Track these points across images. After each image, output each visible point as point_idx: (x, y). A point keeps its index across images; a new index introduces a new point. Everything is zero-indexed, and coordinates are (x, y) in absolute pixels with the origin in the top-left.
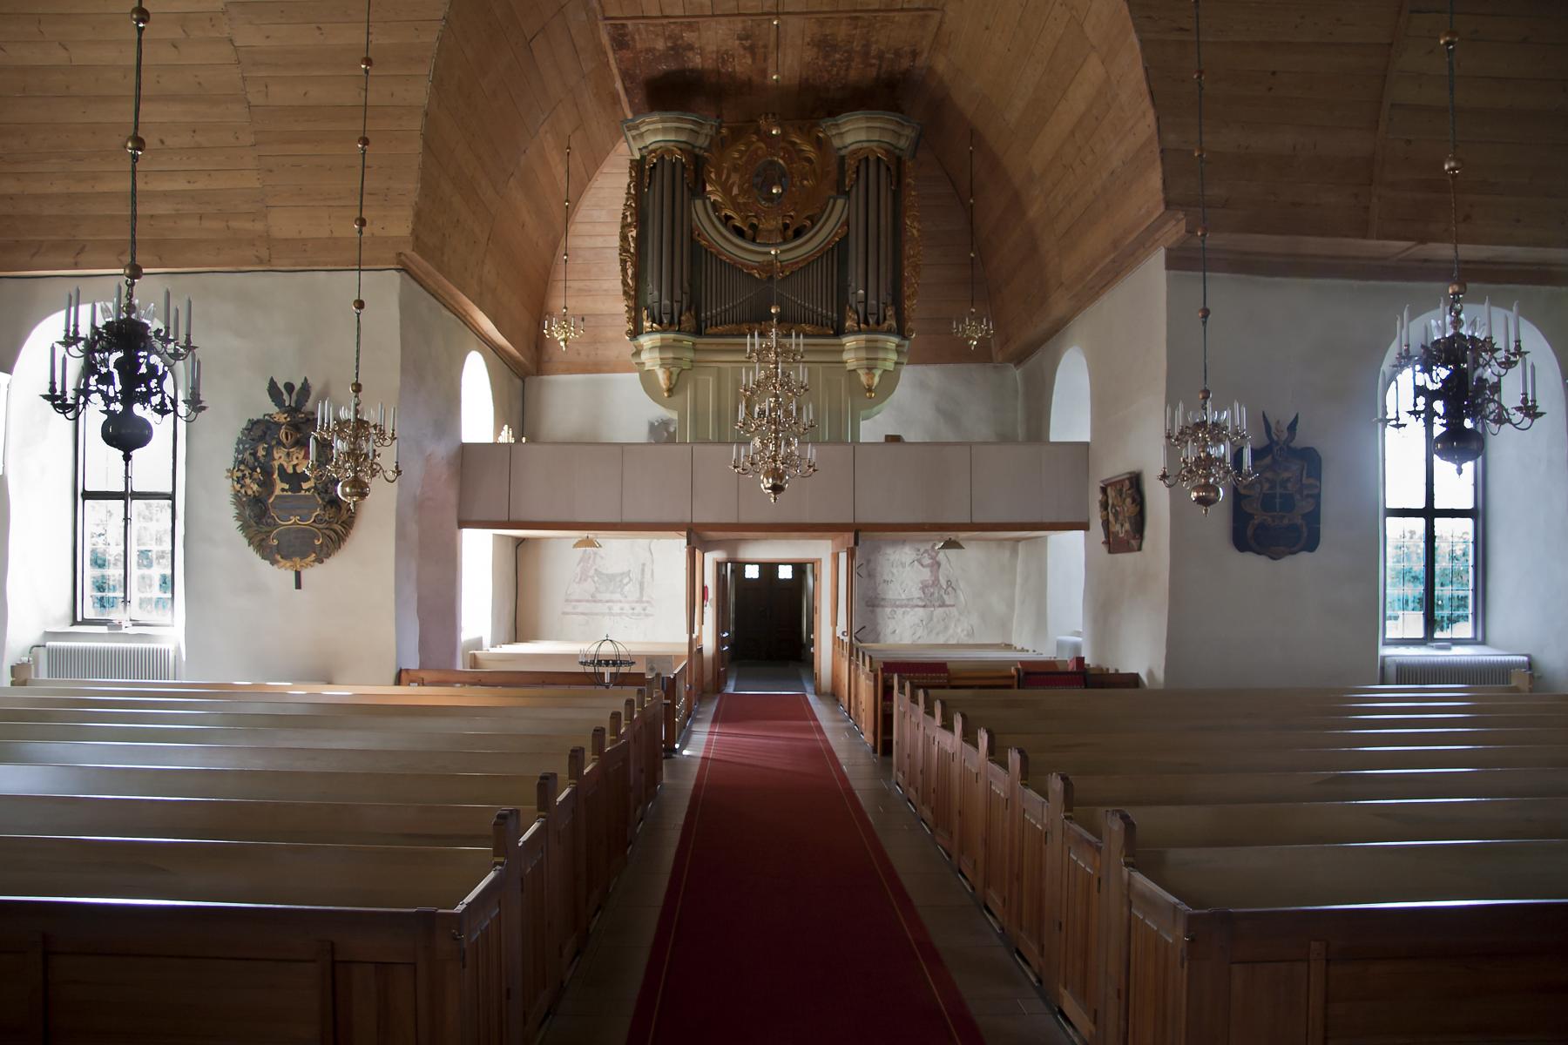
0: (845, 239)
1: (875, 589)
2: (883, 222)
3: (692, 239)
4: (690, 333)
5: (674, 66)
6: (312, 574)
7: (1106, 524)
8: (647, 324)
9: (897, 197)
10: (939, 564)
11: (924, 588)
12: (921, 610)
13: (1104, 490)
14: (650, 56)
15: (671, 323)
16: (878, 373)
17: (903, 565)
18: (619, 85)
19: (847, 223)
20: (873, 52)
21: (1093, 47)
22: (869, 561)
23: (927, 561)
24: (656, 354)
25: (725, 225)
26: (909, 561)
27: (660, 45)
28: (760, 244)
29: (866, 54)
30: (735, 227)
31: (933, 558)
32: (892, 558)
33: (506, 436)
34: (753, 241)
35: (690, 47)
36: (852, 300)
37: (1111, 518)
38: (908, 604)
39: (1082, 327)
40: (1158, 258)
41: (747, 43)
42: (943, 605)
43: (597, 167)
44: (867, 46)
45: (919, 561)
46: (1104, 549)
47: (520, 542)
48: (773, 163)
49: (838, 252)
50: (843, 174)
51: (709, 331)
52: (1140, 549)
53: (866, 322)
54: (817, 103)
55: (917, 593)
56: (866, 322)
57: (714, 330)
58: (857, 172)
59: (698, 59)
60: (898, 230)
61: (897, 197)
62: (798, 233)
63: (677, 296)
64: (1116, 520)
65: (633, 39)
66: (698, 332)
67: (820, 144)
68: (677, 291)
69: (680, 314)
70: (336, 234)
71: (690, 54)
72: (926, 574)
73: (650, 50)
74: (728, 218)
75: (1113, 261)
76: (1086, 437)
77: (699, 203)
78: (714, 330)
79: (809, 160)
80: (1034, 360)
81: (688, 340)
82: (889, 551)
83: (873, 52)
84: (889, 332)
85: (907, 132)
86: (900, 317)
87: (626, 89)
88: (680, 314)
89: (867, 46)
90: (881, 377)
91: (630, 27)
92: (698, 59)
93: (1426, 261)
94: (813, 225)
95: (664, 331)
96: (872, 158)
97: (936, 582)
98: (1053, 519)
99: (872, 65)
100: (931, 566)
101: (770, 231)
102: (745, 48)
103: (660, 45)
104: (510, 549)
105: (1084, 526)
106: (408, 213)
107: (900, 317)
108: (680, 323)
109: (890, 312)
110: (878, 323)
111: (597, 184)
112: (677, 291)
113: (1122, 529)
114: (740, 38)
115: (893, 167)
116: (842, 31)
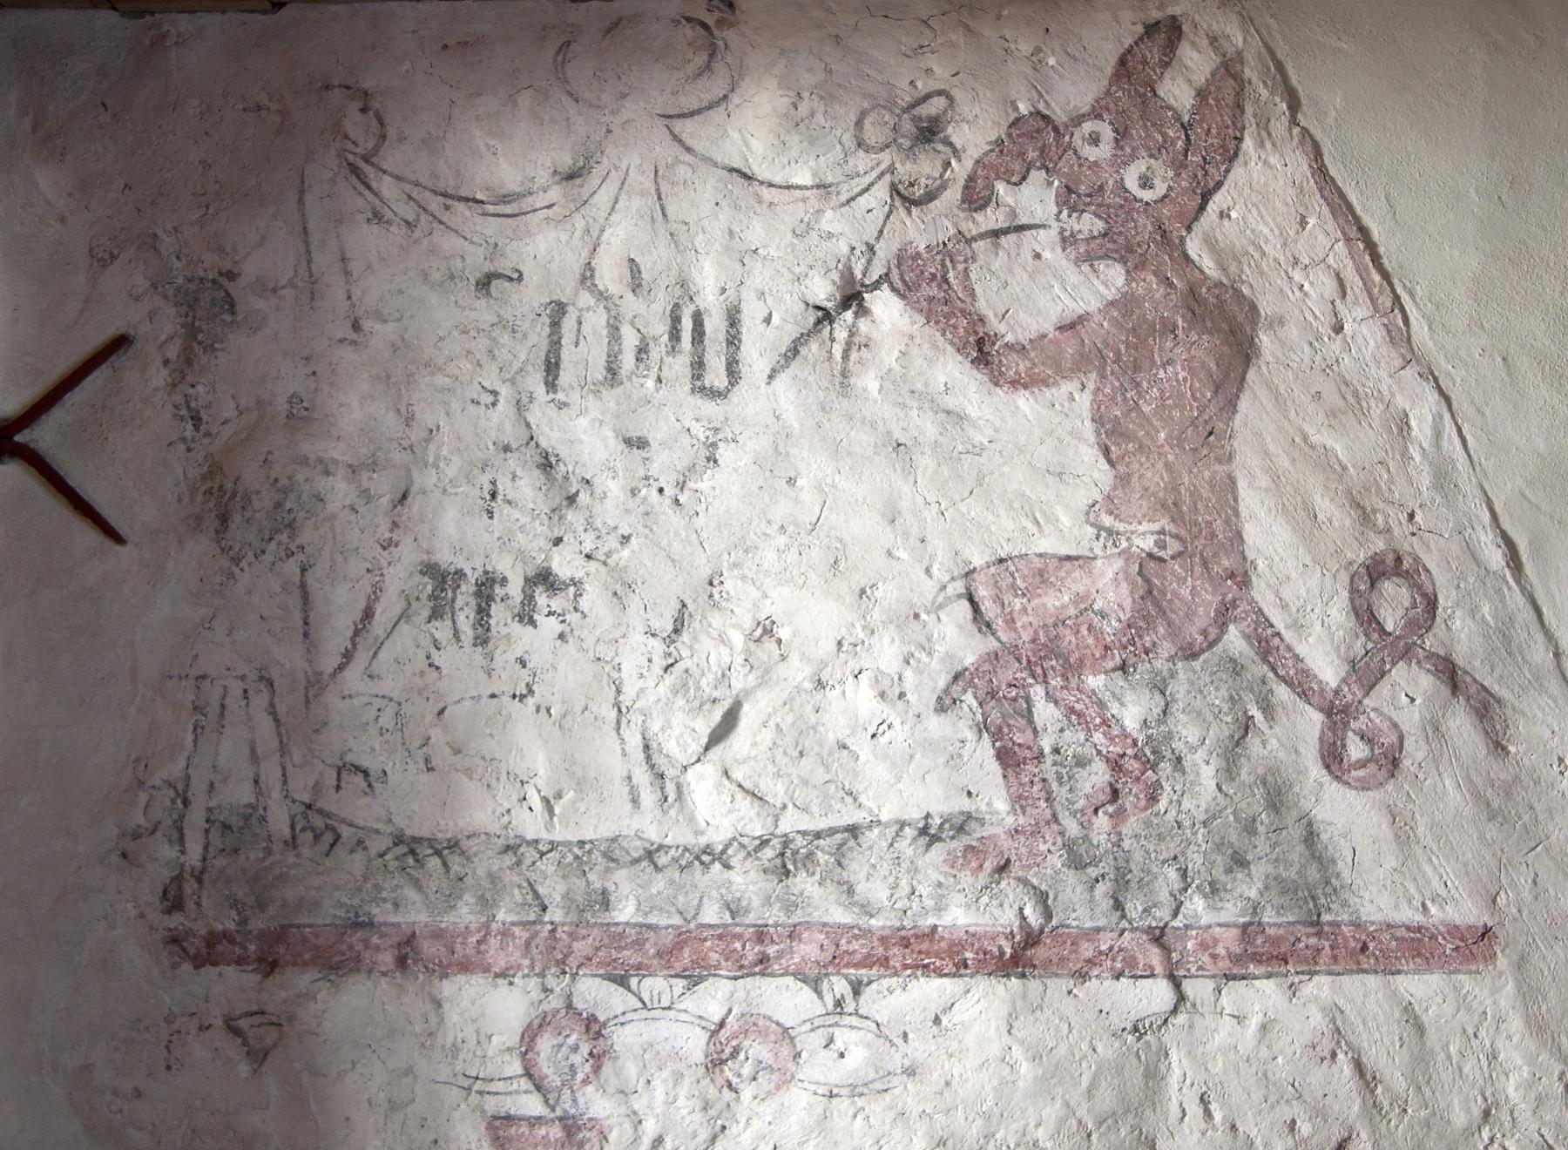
1: (298, 704)
6: (1266, 307)
10: (1227, 327)
11: (1013, 674)
12: (981, 1005)
17: (703, 346)
22: (210, 305)
23: (1046, 282)
26: (781, 291)
31: (1131, 238)
32: (545, 250)
38: (796, 926)
42: (1306, 934)
45: (935, 287)
55: (912, 766)
72: (1038, 479)
82: (513, 155)
93: (1357, 614)
97: (1191, 586)
100: (1105, 357)
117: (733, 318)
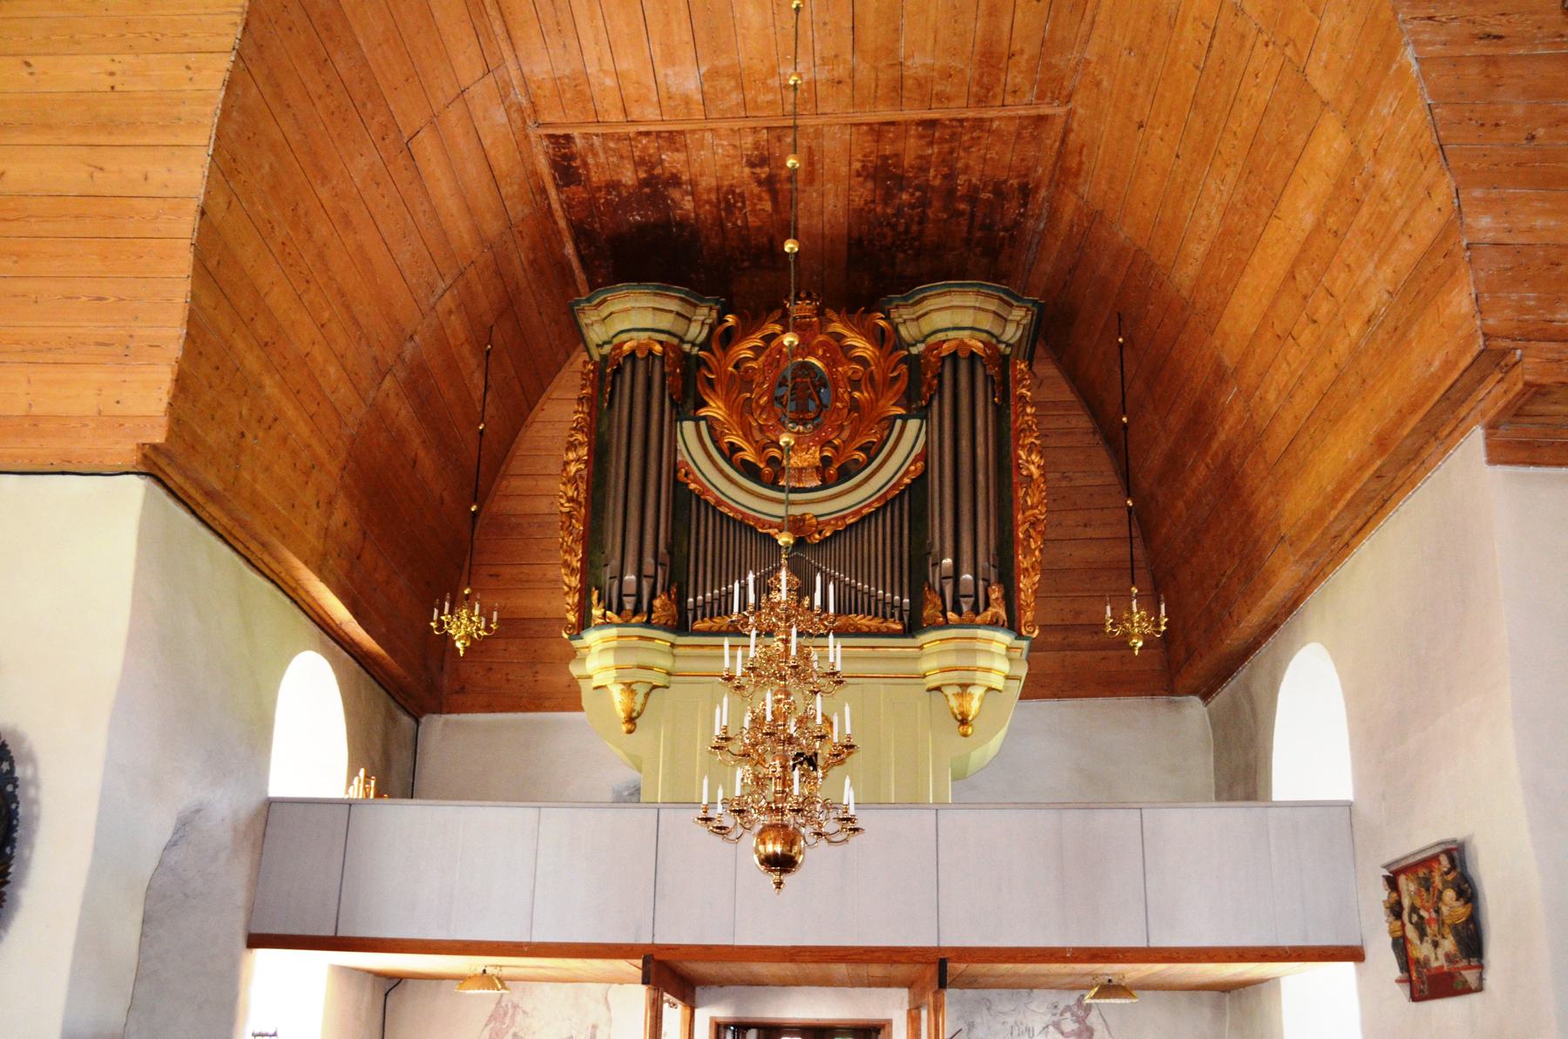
0: (921, 480)
2: (980, 451)
3: (676, 481)
4: (665, 628)
5: (652, 215)
7: (1400, 945)
8: (597, 612)
9: (1001, 414)
10: (1090, 1031)
13: (1392, 882)
14: (613, 197)
15: (637, 611)
16: (977, 692)
18: (569, 249)
19: (924, 456)
20: (961, 191)
21: (1325, 104)
24: (609, 660)
25: (729, 461)
27: (628, 176)
28: (782, 489)
29: (951, 192)
30: (745, 462)
31: (1081, 1021)
33: (356, 792)
34: (774, 485)
35: (675, 181)
36: (934, 577)
37: (1411, 933)
39: (1320, 609)
40: (1475, 440)
41: (763, 172)
43: (543, 389)
44: (950, 177)
45: (1057, 1025)
46: (1402, 993)
47: (392, 983)
48: (806, 366)
49: (911, 499)
50: (921, 381)
51: (699, 625)
52: (1480, 989)
53: (957, 608)
54: (877, 264)
56: (957, 608)
57: (707, 624)
58: (940, 376)
59: (688, 203)
60: (1004, 466)
61: (1001, 414)
62: (845, 474)
63: (649, 568)
64: (1422, 934)
65: (585, 164)
66: (680, 625)
67: (879, 338)
68: (649, 560)
69: (653, 596)
70: (35, 411)
71: (676, 194)
73: (613, 186)
74: (734, 448)
75: (1378, 476)
76: (1345, 793)
77: (688, 426)
78: (707, 624)
79: (862, 361)
80: (1242, 673)
81: (663, 638)
83: (961, 191)
84: (994, 624)
85: (1018, 314)
86: (1010, 599)
87: (581, 258)
88: (653, 596)
89: (950, 177)
90: (982, 700)
91: (579, 143)
92: (688, 203)
94: (870, 460)
95: (626, 624)
96: (963, 354)
98: (1298, 942)
99: (962, 213)
101: (800, 470)
102: (760, 182)
103: (628, 176)
104: (368, 996)
105: (1354, 954)
106: (163, 377)
107: (1010, 599)
108: (651, 610)
109: (995, 594)
110: (975, 610)
111: (541, 416)
112: (649, 560)
113: (1437, 953)
114: (752, 165)
115: (995, 366)
116: (911, 149)
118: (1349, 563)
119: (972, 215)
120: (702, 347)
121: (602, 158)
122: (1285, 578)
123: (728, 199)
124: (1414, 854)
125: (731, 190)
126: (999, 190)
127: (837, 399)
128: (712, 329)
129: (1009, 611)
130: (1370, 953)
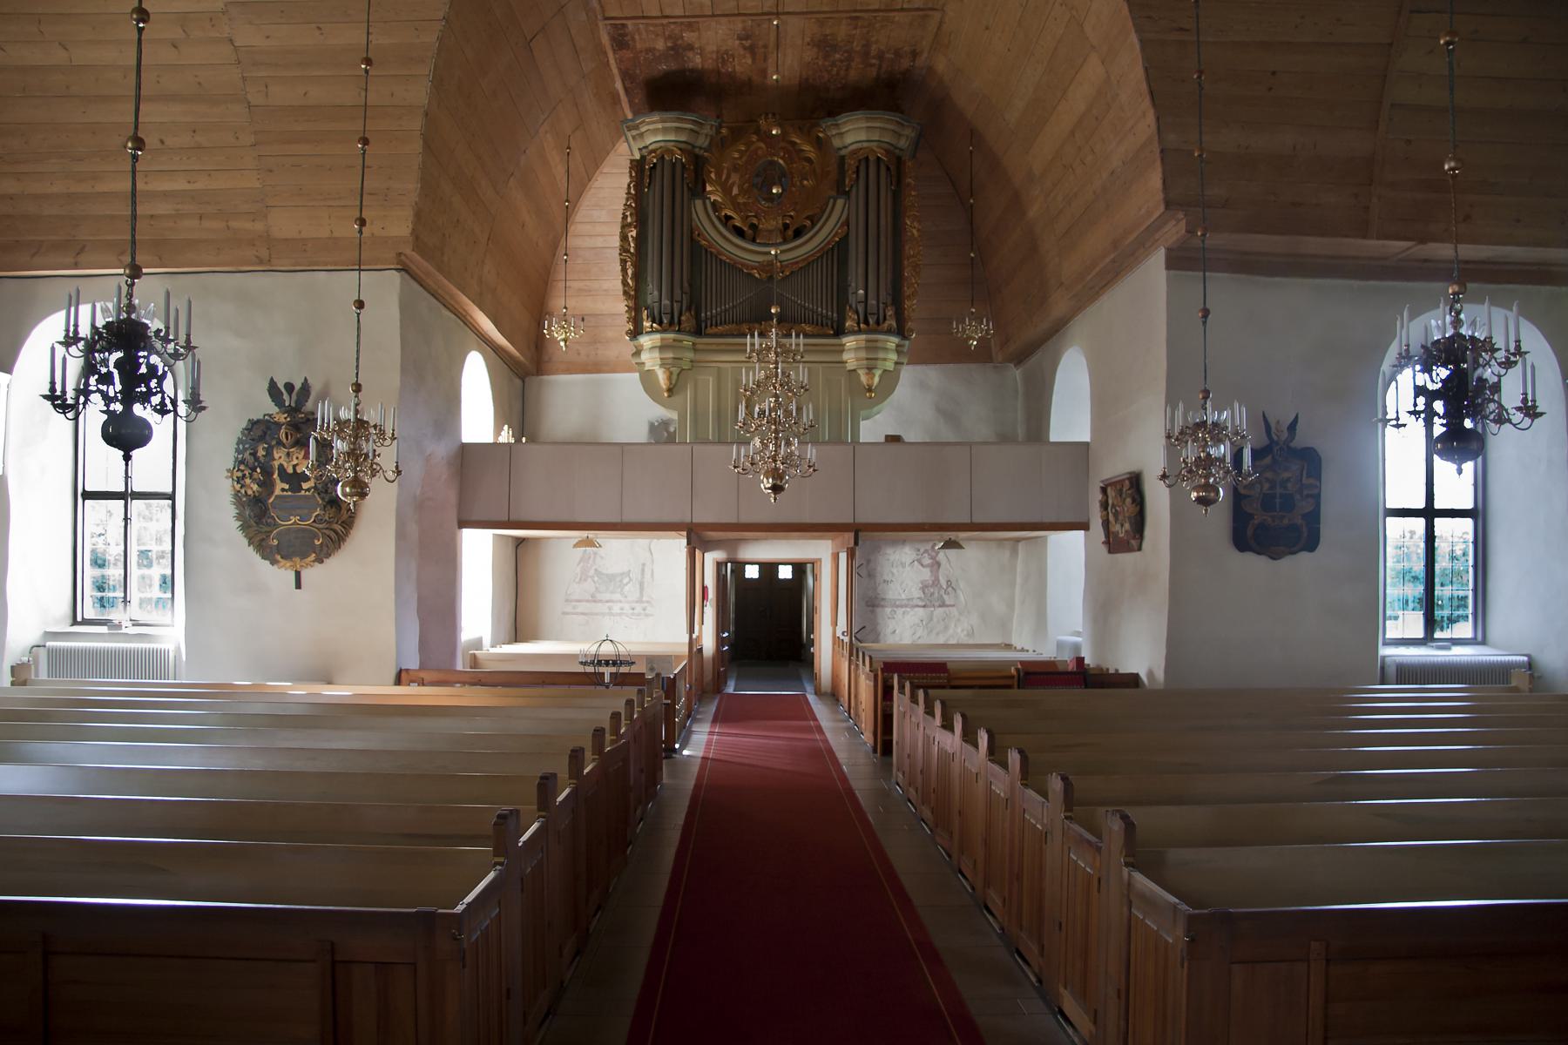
0: (845, 239)
1: (875, 589)
2: (883, 222)
3: (692, 239)
4: (690, 333)
5: (674, 66)
6: (311, 574)
7: (1106, 524)
8: (647, 324)
9: (897, 197)
10: (939, 564)
11: (924, 588)
12: (921, 610)
13: (1104, 490)
14: (650, 56)
15: (671, 323)
16: (878, 373)
17: (903, 565)
18: (619, 85)
19: (847, 223)
21: (1093, 47)
22: (869, 561)
23: (927, 561)
24: (656, 354)
25: (725, 225)
26: (909, 561)
27: (660, 45)
28: (760, 244)
29: (866, 54)
30: (735, 227)
31: (933, 558)
32: (892, 558)
33: (506, 436)
34: (753, 241)
35: (690, 47)
36: (852, 300)
37: (1111, 518)
38: (908, 604)
39: (1081, 327)
40: (1158, 258)
41: (747, 43)
42: (943, 605)
43: (597, 167)
44: (867, 46)
45: (919, 561)
46: (1104, 549)
47: (520, 542)
48: (772, 163)
49: (838, 252)
50: (843, 174)
51: (709, 331)
52: (1140, 549)
53: (866, 322)
54: (817, 103)
55: (917, 593)
56: (866, 322)
58: (857, 172)
59: (698, 59)
60: (898, 230)
61: (897, 197)
62: (798, 233)
63: (677, 296)
64: (1116, 520)
65: (633, 39)
66: (698, 332)
67: (820, 144)
68: (677, 292)
69: (680, 314)
70: (336, 234)
71: (690, 54)
72: (926, 574)
73: (650, 50)
74: (728, 218)
75: (1113, 261)
77: (699, 203)
79: (809, 160)
80: (1034, 359)
81: (688, 340)
82: (889, 551)
84: (889, 332)
85: (907, 132)
87: (626, 89)
88: (680, 314)
89: (867, 46)
90: (881, 377)
91: (630, 27)
92: (698, 59)
94: (813, 225)
95: (664, 331)
96: (872, 158)
97: (936, 582)
99: (872, 65)
100: (931, 566)
101: (770, 231)
102: (745, 48)
103: (660, 45)
104: (510, 549)
105: (1084, 526)
106: (408, 213)
107: (900, 317)
108: (680, 323)
109: (890, 312)
110: (878, 323)
111: (597, 184)
112: (677, 292)
113: (1122, 529)
114: (740, 38)
115: (894, 166)
116: (842, 31)
117: (255, 133)
118: (1097, 304)
119: (880, 67)
120: (706, 150)
121: (644, 35)
122: (1059, 305)
123: (724, 56)
124: (945, 646)
125: (726, 52)
126: (897, 53)
127: (793, 185)
128: (712, 138)
129: (898, 322)
130: (1092, 526)
